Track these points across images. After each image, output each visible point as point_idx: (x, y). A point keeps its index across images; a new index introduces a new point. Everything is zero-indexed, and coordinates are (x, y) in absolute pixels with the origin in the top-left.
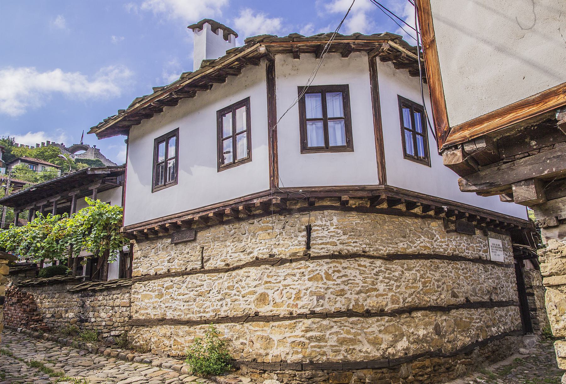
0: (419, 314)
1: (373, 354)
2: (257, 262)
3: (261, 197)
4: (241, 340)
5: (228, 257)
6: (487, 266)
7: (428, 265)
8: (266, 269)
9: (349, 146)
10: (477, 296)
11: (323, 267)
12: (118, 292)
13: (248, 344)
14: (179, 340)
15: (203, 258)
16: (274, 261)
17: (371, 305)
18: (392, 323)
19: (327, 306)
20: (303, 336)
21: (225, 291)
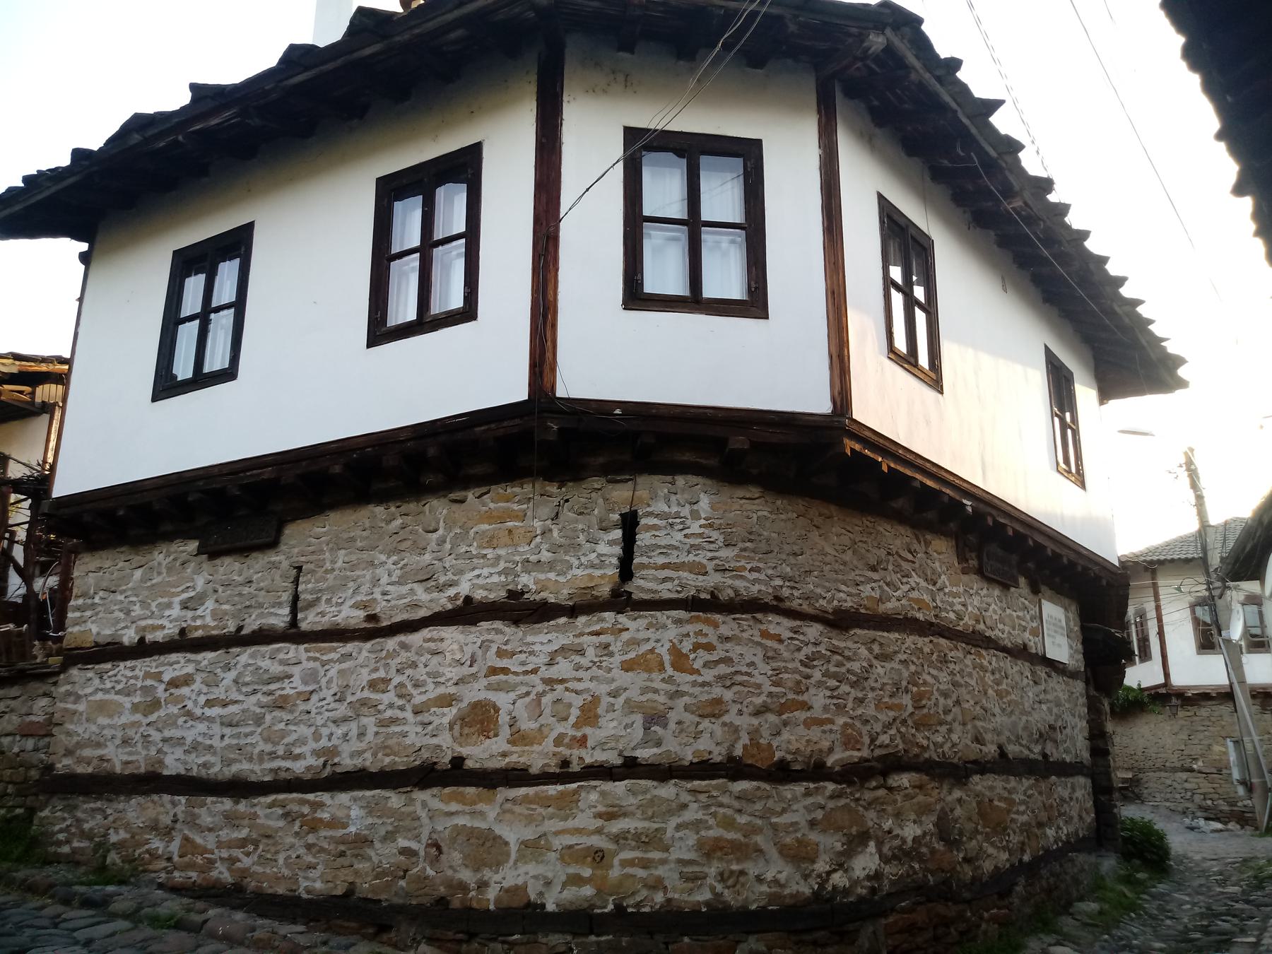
0: (904, 780)
1: (793, 888)
2: (467, 613)
4: (403, 843)
5: (378, 596)
6: (1038, 668)
7: (927, 650)
8: (498, 631)
9: (754, 304)
10: (1021, 745)
11: (664, 634)
12: (15, 691)
13: (422, 853)
14: (199, 840)
15: (296, 598)
16: (521, 610)
17: (793, 748)
18: (842, 802)
20: (599, 831)
21: (359, 695)
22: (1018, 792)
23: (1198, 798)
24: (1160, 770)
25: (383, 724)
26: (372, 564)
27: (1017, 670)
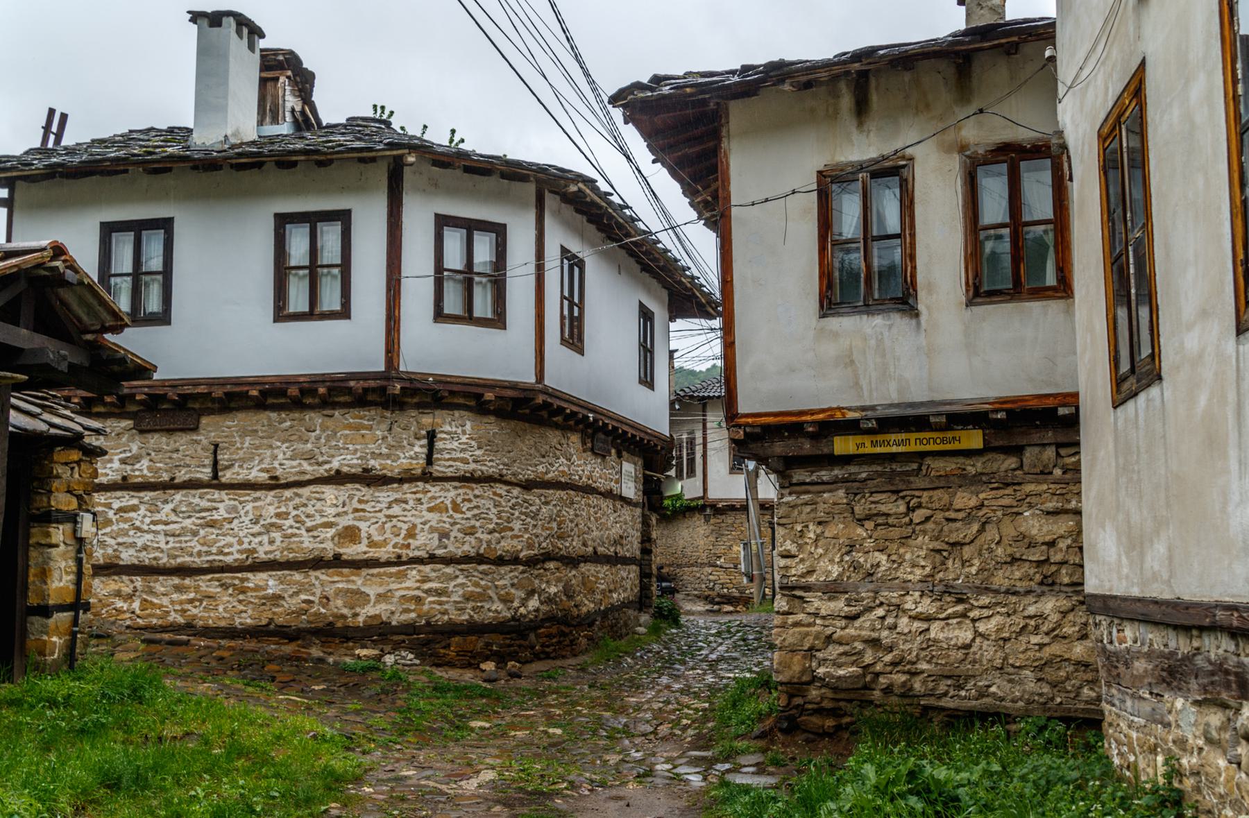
0: (551, 565)
2: (338, 478)
3: (366, 380)
4: (303, 597)
8: (358, 490)
9: (498, 320)
11: (449, 494)
16: (369, 478)
19: (451, 548)
20: (418, 588)
21: (269, 521)
22: (601, 574)
23: (717, 587)
24: (692, 565)
25: (286, 536)
26: (271, 447)
27: (606, 504)
